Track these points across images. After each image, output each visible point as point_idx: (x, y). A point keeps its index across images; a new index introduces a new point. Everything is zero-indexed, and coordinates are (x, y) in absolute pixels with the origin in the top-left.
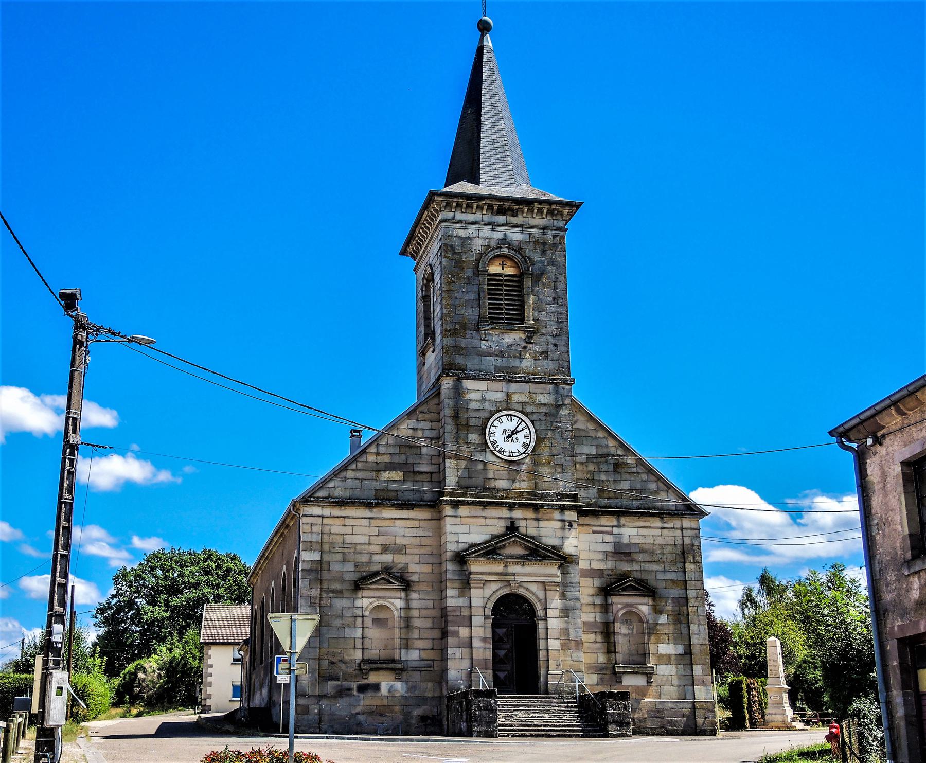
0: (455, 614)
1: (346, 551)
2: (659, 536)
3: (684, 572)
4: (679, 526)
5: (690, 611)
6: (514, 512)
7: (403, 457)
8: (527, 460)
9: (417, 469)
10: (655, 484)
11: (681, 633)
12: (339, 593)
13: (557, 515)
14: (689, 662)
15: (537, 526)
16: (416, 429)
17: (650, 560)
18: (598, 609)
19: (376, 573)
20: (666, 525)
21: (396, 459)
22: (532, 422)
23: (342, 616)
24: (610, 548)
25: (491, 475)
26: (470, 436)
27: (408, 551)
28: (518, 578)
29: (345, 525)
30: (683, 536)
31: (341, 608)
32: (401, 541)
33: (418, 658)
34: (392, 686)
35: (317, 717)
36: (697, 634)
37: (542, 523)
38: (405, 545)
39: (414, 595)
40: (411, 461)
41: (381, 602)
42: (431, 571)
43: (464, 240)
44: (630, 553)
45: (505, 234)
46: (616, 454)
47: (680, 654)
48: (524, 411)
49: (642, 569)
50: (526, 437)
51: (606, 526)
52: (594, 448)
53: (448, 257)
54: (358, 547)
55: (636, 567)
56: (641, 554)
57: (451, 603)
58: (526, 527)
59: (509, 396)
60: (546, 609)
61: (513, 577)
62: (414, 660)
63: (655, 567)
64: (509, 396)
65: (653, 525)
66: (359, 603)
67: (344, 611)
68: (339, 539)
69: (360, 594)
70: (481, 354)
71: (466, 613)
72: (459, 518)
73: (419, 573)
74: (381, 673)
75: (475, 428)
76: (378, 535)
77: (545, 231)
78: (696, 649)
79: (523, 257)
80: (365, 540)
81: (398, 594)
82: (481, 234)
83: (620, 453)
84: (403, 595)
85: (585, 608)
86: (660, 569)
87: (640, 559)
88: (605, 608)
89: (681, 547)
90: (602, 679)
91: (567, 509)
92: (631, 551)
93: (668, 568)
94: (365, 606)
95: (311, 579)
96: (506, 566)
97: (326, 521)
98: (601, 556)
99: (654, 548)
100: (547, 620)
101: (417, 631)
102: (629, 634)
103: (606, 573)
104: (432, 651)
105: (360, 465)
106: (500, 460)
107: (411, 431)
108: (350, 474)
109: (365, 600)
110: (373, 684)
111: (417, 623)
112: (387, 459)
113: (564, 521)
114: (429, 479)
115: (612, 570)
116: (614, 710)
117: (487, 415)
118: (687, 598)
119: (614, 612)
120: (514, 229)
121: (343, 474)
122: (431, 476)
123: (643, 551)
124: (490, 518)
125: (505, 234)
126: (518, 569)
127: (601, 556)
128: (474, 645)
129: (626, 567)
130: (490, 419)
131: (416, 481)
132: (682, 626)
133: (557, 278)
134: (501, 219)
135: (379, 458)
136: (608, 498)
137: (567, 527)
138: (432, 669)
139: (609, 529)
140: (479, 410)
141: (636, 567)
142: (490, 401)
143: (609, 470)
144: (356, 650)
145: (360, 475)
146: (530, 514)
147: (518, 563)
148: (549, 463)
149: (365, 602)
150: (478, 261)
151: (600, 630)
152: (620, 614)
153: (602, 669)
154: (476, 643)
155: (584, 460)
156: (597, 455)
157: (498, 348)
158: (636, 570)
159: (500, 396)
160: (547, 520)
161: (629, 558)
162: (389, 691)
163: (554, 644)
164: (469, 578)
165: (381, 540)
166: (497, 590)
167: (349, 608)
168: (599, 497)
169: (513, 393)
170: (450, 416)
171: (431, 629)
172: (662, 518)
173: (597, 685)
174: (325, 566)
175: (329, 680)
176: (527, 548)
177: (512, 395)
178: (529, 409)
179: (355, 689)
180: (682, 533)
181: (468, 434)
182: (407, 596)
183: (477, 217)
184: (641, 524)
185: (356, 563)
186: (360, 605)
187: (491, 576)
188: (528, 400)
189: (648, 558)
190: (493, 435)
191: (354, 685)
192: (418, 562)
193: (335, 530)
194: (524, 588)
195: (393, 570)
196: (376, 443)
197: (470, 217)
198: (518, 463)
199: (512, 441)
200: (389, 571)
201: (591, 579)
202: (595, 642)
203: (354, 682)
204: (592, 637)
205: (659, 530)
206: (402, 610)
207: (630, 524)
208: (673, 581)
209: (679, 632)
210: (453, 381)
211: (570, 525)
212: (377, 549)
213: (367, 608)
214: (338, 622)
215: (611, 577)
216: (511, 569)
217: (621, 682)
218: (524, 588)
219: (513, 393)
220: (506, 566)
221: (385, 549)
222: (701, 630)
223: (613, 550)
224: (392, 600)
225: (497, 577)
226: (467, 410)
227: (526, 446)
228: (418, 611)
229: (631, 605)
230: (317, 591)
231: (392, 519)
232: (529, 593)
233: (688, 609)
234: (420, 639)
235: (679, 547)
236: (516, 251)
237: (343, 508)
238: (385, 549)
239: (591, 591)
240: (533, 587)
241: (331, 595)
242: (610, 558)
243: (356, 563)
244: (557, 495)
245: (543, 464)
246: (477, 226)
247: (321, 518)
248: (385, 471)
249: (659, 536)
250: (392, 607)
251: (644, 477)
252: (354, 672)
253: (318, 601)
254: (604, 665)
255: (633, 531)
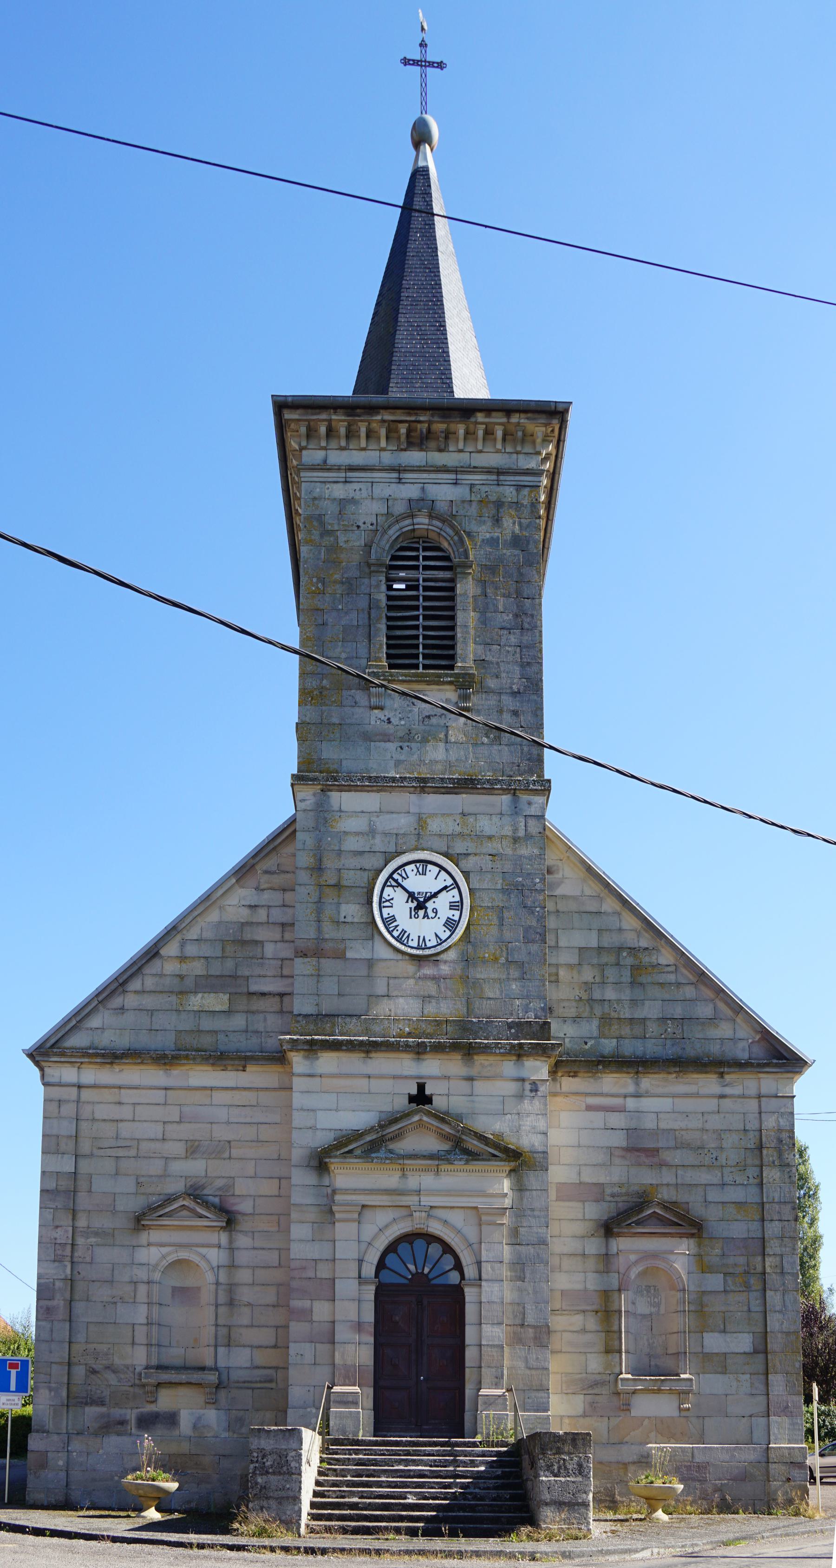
0: (304, 1275)
1: (121, 1153)
2: (713, 1113)
3: (761, 1185)
4: (753, 1092)
5: (767, 1264)
6: (425, 1063)
7: (230, 964)
8: (452, 955)
9: (254, 988)
10: (711, 1006)
11: (749, 1311)
12: (107, 1236)
13: (509, 1067)
14: (761, 1368)
15: (469, 1092)
16: (256, 906)
17: (696, 1163)
18: (591, 1264)
19: (170, 1199)
20: (728, 1091)
21: (216, 969)
22: (466, 874)
23: (111, 1282)
24: (619, 1140)
25: (380, 988)
26: (343, 907)
27: (235, 1153)
28: (426, 1201)
29: (120, 1103)
30: (760, 1113)
31: (110, 1265)
32: (222, 1133)
33: (248, 1365)
34: (199, 1418)
35: (63, 1474)
36: (780, 1312)
37: (480, 1086)
38: (229, 1142)
39: (242, 1241)
40: (244, 971)
41: (183, 1254)
42: (277, 1194)
43: (343, 503)
44: (657, 1150)
45: (423, 489)
46: (636, 946)
47: (745, 1353)
48: (450, 851)
49: (679, 1181)
50: (453, 906)
51: (612, 1096)
52: (594, 934)
53: (311, 541)
54: (144, 1146)
55: (667, 1177)
56: (678, 1151)
57: (301, 1251)
58: (448, 1095)
59: (421, 822)
60: (479, 1263)
61: (416, 1198)
62: (241, 1368)
63: (704, 1177)
64: (421, 822)
65: (704, 1091)
66: (142, 1255)
67: (116, 1272)
68: (108, 1130)
69: (144, 1237)
70: (368, 737)
71: (324, 1272)
72: (318, 1079)
73: (254, 1197)
74: (182, 1391)
75: (354, 890)
76: (180, 1122)
77: (502, 478)
78: (775, 1344)
79: (457, 533)
80: (155, 1130)
81: (211, 1237)
82: (378, 490)
83: (644, 944)
84: (224, 1238)
85: (566, 1263)
86: (716, 1181)
87: (677, 1161)
88: (606, 1260)
89: (757, 1134)
90: (592, 1404)
91: (528, 1055)
92: (660, 1145)
93: (728, 1179)
94: (153, 1261)
95: (56, 1209)
96: (404, 1176)
97: (86, 1094)
98: (600, 1158)
99: (705, 1137)
100: (480, 1286)
101: (246, 1311)
102: (651, 1315)
103: (608, 1191)
104: (273, 1350)
105: (150, 983)
106: (400, 956)
107: (245, 912)
108: (130, 1000)
109: (153, 1250)
110: (165, 1413)
111: (245, 1295)
112: (197, 968)
113: (523, 1080)
114: (277, 1008)
115: (621, 1186)
116: (555, 1476)
117: (377, 861)
118: (764, 1238)
119: (622, 1271)
120: (440, 476)
121: (117, 1001)
122: (282, 1002)
123: (681, 1146)
124: (382, 1077)
125: (423, 489)
126: (428, 1180)
127: (600, 1158)
128: (338, 1338)
129: (646, 1177)
130: (381, 871)
131: (253, 1012)
132: (753, 1295)
133: (521, 574)
134: (415, 457)
135: (184, 966)
136: (619, 1038)
137: (527, 1093)
138: (273, 1385)
139: (618, 1101)
140: (362, 853)
141: (667, 1177)
142: (385, 834)
143: (624, 979)
144: (135, 1346)
145: (148, 1001)
146: (454, 1065)
147: (427, 1170)
148: (496, 960)
149: (153, 1255)
150: (368, 546)
151: (594, 1307)
152: (633, 1273)
153: (595, 1384)
154: (343, 1333)
155: (574, 960)
156: (600, 949)
157: (403, 722)
158: (668, 1185)
159: (403, 823)
160: (488, 1078)
161: (656, 1160)
162: (195, 1427)
163: (493, 1333)
164: (333, 1201)
165: (186, 1131)
166: (387, 1226)
167: (125, 1265)
168: (602, 1035)
169: (433, 815)
170: (307, 868)
171: (274, 1306)
172: (721, 1075)
173: (584, 1415)
174: (82, 1184)
175: (86, 1404)
176: (446, 1137)
177: (429, 821)
178: (459, 847)
179: (133, 1422)
180: (760, 1106)
181: (339, 904)
182: (231, 1241)
183: (370, 457)
184: (681, 1088)
185: (137, 1177)
186: (144, 1260)
187: (374, 1197)
188: (458, 829)
189: (690, 1158)
190: (387, 904)
191: (131, 1415)
192: (252, 1174)
193: (101, 1112)
194: (439, 1219)
195: (206, 1192)
196: (179, 937)
197: (356, 457)
198: (433, 959)
199: (426, 916)
200: (197, 1192)
201: (580, 1205)
202: (584, 1331)
203: (132, 1409)
204: (577, 1321)
205: (715, 1101)
206: (221, 1271)
207: (660, 1090)
208: (739, 1205)
209: (746, 1308)
210: (314, 795)
211: (535, 1089)
212: (178, 1149)
213: (157, 1265)
214: (102, 1293)
215: (616, 1199)
216: (413, 1182)
217: (629, 1410)
218: (439, 1219)
219: (433, 815)
220: (404, 1176)
221: (193, 1149)
222: (788, 1303)
223: (624, 1144)
224: (203, 1251)
225: (385, 1197)
226: (340, 853)
227: (451, 925)
228: (250, 1271)
229: (655, 1255)
230: (66, 1231)
231: (205, 1088)
232: (448, 1232)
233: (764, 1260)
234: (252, 1326)
235: (751, 1135)
236: (444, 521)
237: (117, 1068)
238: (193, 1149)
239: (579, 1228)
240: (457, 1218)
241: (92, 1240)
242: (617, 1161)
243: (137, 1177)
244: (510, 1026)
245: (484, 961)
246: (368, 474)
247: (76, 1089)
248: (196, 993)
249: (713, 1113)
250: (203, 1265)
251: (689, 992)
252: (131, 1389)
253: (68, 1251)
254: (598, 1377)
255: (664, 1104)
